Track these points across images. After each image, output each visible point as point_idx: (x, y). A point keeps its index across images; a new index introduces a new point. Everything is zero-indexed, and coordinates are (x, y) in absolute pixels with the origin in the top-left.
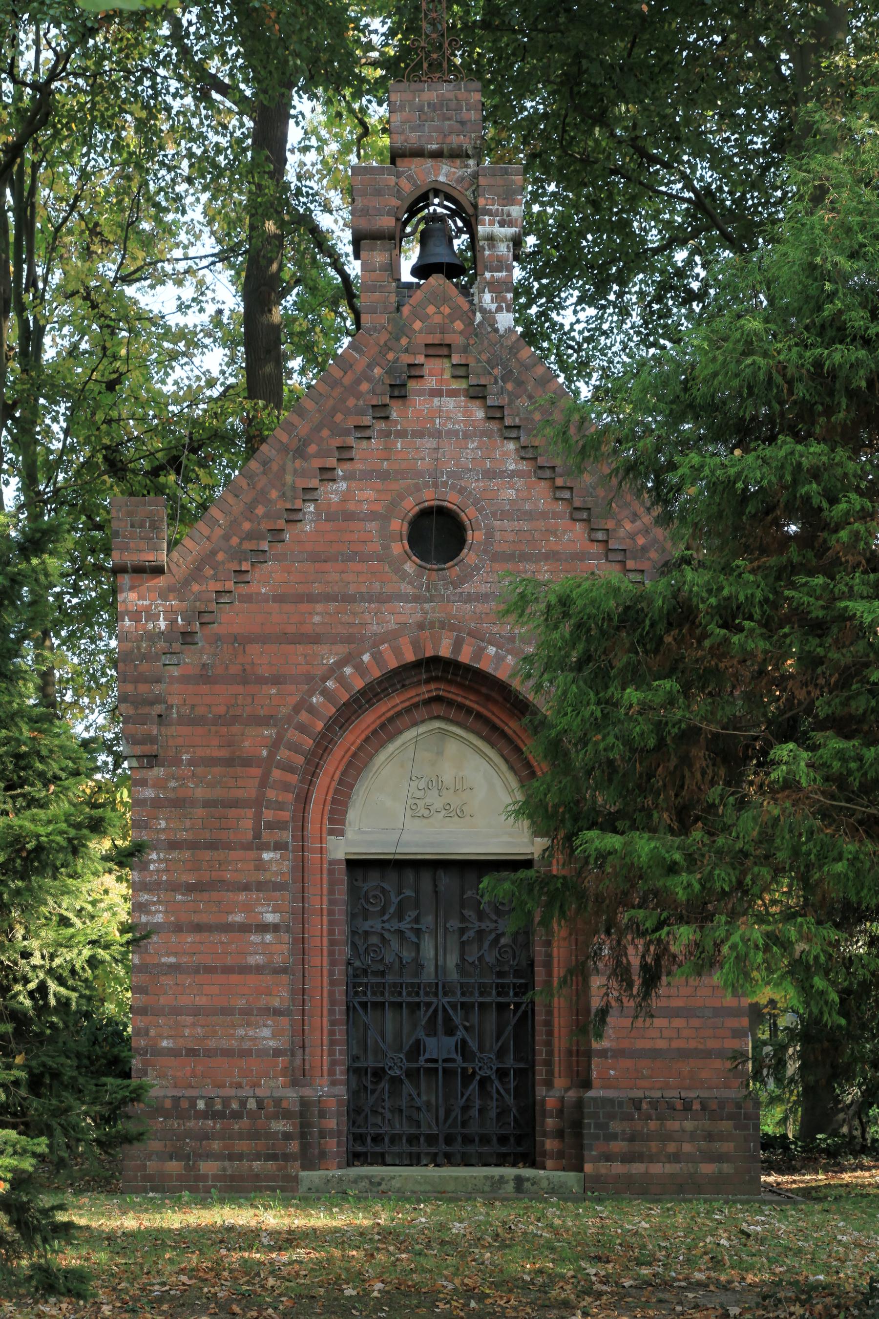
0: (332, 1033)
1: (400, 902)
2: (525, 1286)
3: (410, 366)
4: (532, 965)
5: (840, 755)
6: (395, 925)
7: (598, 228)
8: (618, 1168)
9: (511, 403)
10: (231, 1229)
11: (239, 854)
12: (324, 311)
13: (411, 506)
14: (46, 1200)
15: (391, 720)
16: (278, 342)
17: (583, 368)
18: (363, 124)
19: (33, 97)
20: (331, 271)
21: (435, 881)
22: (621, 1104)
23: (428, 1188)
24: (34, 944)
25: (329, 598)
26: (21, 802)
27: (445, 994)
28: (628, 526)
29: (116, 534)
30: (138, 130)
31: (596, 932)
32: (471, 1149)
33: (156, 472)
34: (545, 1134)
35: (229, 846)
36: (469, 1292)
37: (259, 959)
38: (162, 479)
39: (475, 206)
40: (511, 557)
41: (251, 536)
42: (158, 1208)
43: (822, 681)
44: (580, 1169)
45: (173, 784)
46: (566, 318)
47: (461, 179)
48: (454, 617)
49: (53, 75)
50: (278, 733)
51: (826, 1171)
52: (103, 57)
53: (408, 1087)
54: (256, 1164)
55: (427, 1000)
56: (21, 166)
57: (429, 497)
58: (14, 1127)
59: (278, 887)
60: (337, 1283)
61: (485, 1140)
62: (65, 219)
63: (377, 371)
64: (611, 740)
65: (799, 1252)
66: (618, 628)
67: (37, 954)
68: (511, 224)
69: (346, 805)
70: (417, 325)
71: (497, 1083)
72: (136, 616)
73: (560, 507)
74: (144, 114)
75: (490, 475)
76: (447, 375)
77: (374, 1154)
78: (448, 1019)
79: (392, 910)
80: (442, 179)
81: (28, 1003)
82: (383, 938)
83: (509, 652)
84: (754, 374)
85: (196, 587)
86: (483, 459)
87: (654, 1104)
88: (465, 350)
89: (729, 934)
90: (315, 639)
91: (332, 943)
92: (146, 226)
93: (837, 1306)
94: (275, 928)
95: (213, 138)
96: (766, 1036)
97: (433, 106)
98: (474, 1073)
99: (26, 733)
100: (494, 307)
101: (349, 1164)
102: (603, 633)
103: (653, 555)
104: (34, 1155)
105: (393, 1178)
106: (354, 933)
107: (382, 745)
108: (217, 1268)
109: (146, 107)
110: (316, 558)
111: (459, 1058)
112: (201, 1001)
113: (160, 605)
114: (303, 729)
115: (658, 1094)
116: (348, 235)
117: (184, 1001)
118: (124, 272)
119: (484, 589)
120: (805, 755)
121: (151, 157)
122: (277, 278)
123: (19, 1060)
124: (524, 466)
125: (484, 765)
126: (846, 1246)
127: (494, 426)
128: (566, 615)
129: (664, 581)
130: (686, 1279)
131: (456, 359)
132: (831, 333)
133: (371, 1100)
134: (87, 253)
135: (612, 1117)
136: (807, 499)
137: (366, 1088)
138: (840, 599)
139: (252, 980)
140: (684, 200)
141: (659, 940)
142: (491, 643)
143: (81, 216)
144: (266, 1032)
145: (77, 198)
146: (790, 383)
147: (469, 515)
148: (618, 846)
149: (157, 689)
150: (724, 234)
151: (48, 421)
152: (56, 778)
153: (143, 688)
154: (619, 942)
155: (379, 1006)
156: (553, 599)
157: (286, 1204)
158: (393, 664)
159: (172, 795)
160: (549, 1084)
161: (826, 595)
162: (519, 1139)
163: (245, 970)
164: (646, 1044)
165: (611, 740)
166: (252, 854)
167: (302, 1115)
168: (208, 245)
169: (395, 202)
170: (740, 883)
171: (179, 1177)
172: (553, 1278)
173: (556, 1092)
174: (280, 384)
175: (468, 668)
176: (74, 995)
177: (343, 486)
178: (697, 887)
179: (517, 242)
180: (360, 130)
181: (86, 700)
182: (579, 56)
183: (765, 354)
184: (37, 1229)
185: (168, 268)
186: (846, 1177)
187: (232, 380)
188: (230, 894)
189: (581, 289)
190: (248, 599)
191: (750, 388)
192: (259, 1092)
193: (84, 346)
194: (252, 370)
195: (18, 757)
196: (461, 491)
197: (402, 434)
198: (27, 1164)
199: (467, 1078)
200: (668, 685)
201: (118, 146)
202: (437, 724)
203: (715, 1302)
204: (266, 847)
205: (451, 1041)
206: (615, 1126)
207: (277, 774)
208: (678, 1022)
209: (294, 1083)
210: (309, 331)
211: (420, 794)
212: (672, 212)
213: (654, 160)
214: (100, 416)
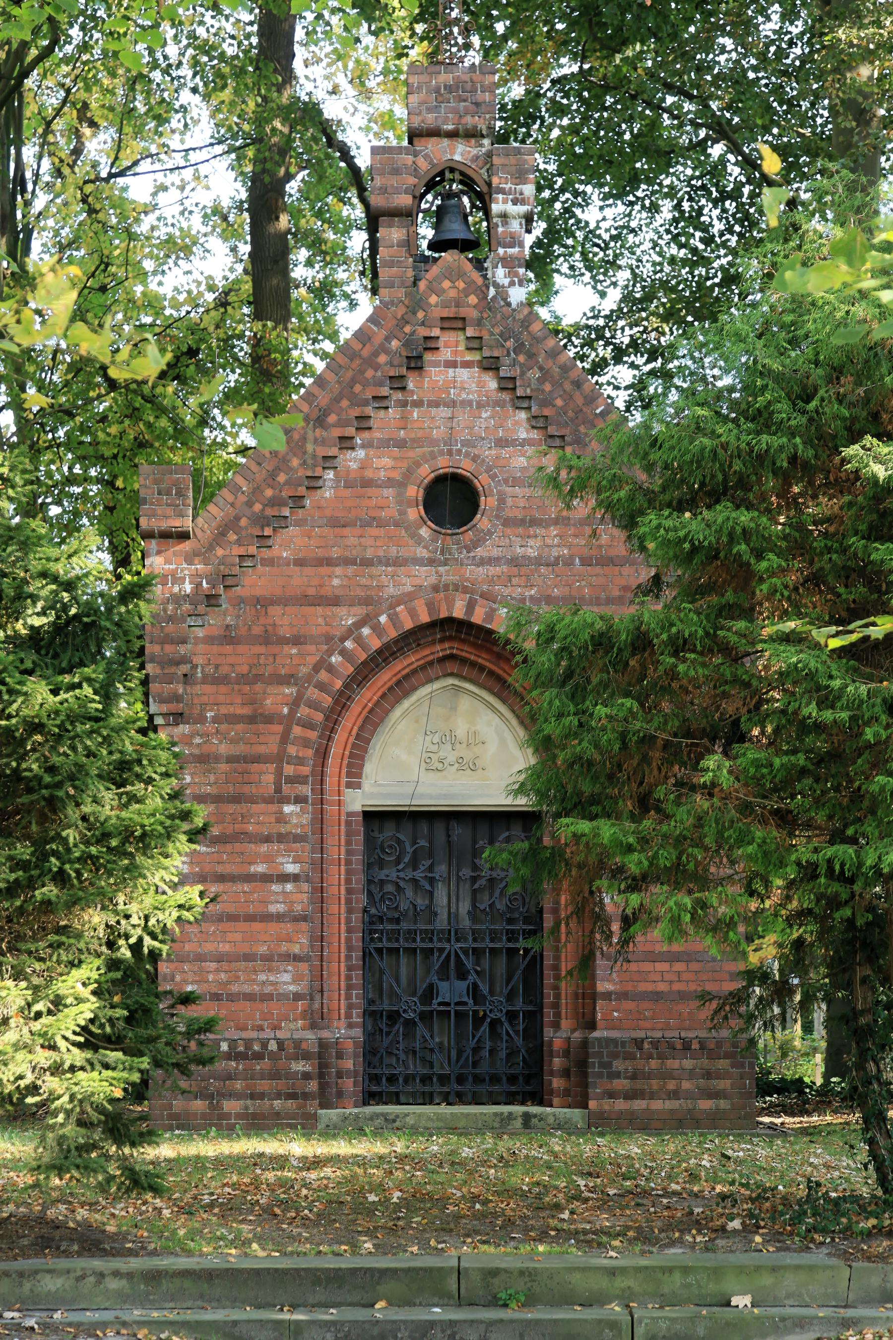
0: (349, 978)
1: (415, 852)
2: (524, 1195)
4: (541, 912)
6: (409, 874)
8: (621, 1105)
9: (523, 374)
10: (262, 1155)
11: (262, 807)
13: (426, 473)
15: (406, 677)
21: (448, 830)
22: (623, 1044)
23: (441, 1124)
24: (133, 908)
25: (349, 562)
27: (458, 940)
32: (482, 1088)
34: (552, 1073)
35: (252, 800)
36: (475, 1198)
37: (280, 908)
39: (489, 184)
40: (522, 522)
44: (586, 1106)
45: (198, 740)
46: (590, 215)
47: (476, 158)
48: (467, 580)
50: (298, 691)
53: (421, 1030)
54: (277, 1103)
55: (439, 945)
57: (443, 464)
59: (297, 838)
61: (495, 1079)
63: (395, 344)
64: (585, 744)
68: (523, 202)
69: (362, 758)
70: (433, 299)
71: (506, 1025)
75: (501, 443)
76: (461, 347)
78: (459, 963)
79: (406, 860)
80: (457, 157)
82: (399, 889)
85: (220, 552)
86: (496, 428)
87: (655, 1044)
88: (479, 323)
90: (335, 601)
91: (349, 891)
94: (295, 878)
97: (449, 88)
98: (485, 1015)
100: (506, 282)
101: (365, 1103)
105: (407, 1115)
106: (370, 882)
110: (336, 523)
111: (471, 1002)
112: (225, 948)
113: (186, 570)
114: (322, 687)
115: (659, 1034)
117: (209, 948)
119: (496, 552)
120: (727, 764)
124: (535, 435)
125: (496, 720)
127: (506, 396)
130: (664, 1189)
131: (470, 332)
135: (615, 1056)
137: (381, 1030)
139: (273, 928)
144: (287, 977)
147: (482, 481)
149: (182, 649)
153: (169, 648)
157: (308, 1136)
158: (409, 625)
159: (196, 752)
160: (556, 1025)
162: (528, 1080)
163: (267, 918)
166: (274, 808)
167: (320, 1055)
169: (412, 180)
171: (204, 1116)
173: (563, 1033)
175: (480, 628)
177: (361, 453)
188: (253, 846)
192: (280, 1035)
196: (475, 458)
197: (418, 404)
199: (478, 1021)
202: (451, 681)
204: (286, 800)
205: (462, 986)
206: (619, 1065)
207: (297, 731)
209: (313, 1026)
211: (434, 748)
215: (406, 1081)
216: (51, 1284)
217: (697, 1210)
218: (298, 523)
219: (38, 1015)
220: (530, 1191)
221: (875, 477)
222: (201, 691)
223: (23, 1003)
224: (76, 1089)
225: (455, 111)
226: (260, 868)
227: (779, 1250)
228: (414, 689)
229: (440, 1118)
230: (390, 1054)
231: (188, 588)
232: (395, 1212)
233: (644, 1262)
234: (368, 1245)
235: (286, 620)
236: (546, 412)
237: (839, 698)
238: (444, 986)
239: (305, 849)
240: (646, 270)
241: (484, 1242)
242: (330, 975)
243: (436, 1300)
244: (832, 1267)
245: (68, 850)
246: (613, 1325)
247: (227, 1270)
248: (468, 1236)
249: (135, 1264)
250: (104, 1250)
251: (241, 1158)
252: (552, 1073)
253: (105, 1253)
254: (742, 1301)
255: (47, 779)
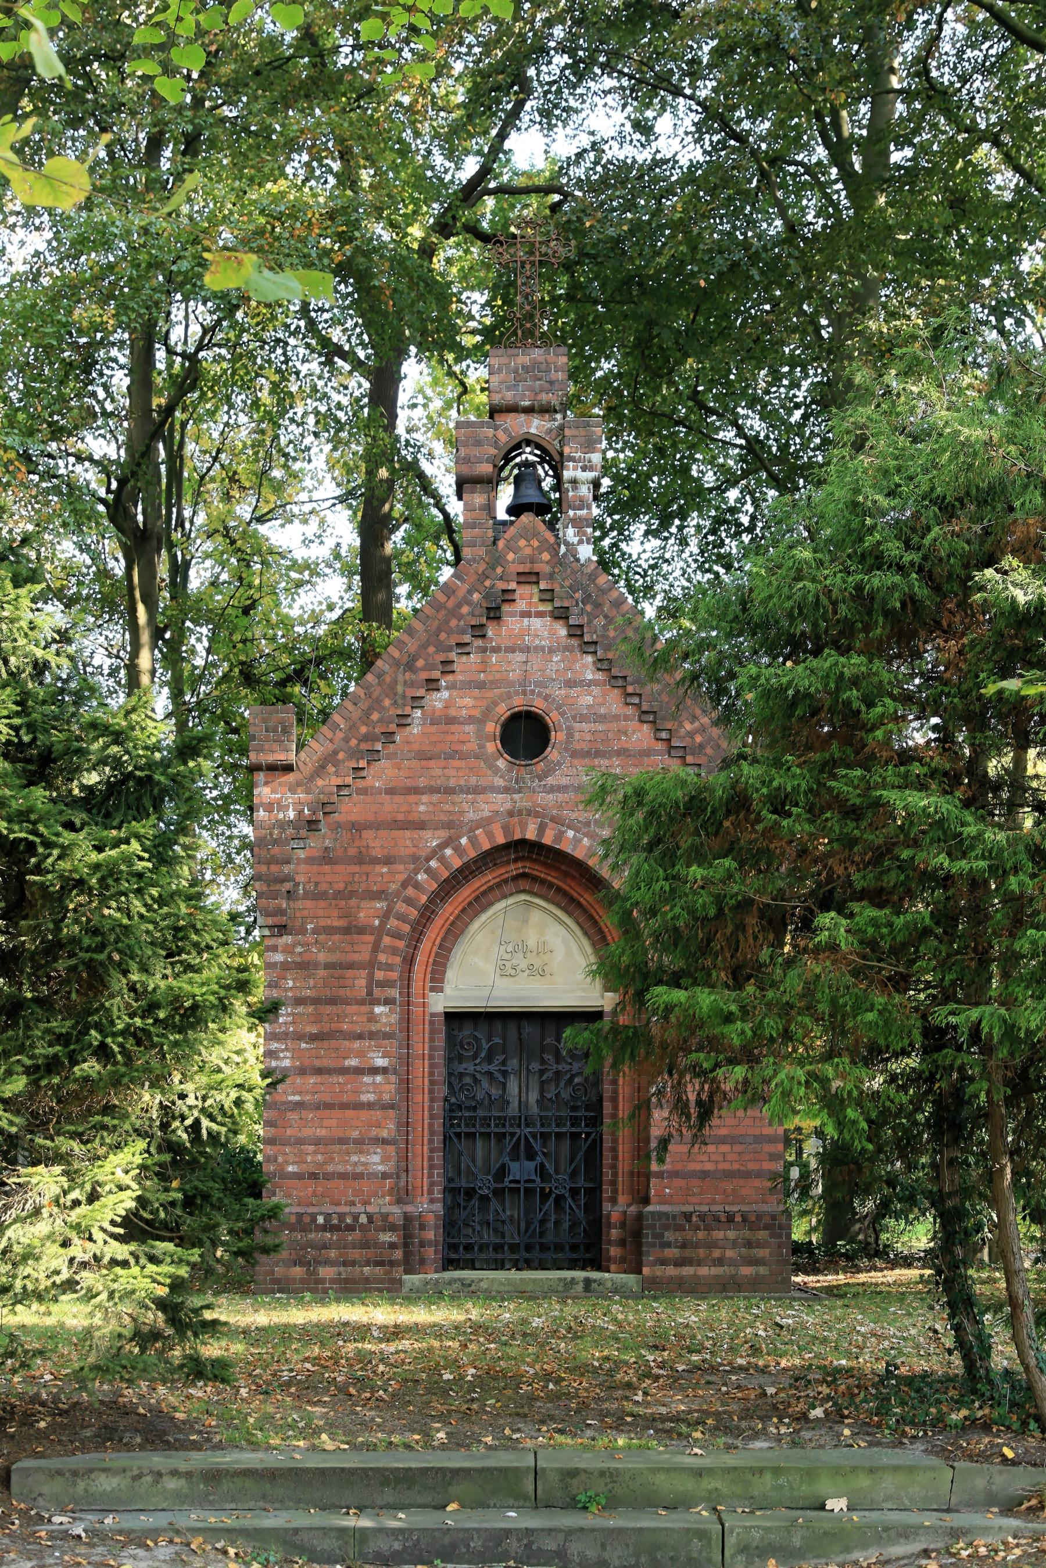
0: (431, 1159)
2: (595, 1371)
3: (504, 591)
4: (600, 1100)
5: (874, 922)
6: (485, 1068)
7: (661, 471)
8: (671, 1271)
9: (590, 622)
10: (346, 1324)
11: (355, 1008)
12: (428, 544)
13: (503, 711)
14: (196, 1301)
15: (484, 893)
16: (390, 572)
17: (648, 591)
18: (462, 384)
19: (183, 365)
20: (435, 511)
22: (674, 1217)
24: (189, 1087)
25: (433, 790)
26: (178, 968)
27: (527, 1125)
28: (688, 727)
29: (253, 738)
30: (272, 392)
31: (660, 1073)
33: (282, 683)
34: (609, 1243)
35: (346, 1002)
36: (548, 1377)
37: (371, 1097)
38: (289, 689)
39: (561, 454)
40: (588, 754)
41: (367, 738)
42: (285, 1306)
43: (857, 859)
44: (639, 1272)
45: (299, 949)
46: (632, 548)
47: (549, 431)
49: (200, 347)
51: (845, 1272)
52: (243, 330)
53: (494, 1204)
54: (366, 1269)
56: (172, 425)
57: (518, 703)
58: (171, 1240)
59: (387, 1036)
60: (436, 1370)
61: (559, 1247)
62: (209, 469)
63: (476, 596)
64: (677, 910)
65: (824, 1341)
66: (684, 815)
67: (192, 1096)
68: (591, 469)
69: (445, 966)
70: (511, 556)
72: (269, 808)
73: (630, 711)
74: (276, 378)
75: (570, 684)
76: (535, 599)
77: (466, 1261)
78: (529, 1146)
80: (533, 431)
81: (185, 1136)
82: (476, 1081)
83: (585, 835)
84: (804, 597)
85: (320, 782)
86: (566, 670)
87: (702, 1217)
88: (551, 577)
89: (776, 1073)
90: (421, 826)
91: (432, 1083)
92: (277, 473)
93: (858, 1387)
94: (384, 1071)
95: (336, 397)
96: (792, 1159)
97: (526, 369)
99: (184, 910)
100: (576, 540)
101: (445, 1269)
102: (671, 819)
103: (709, 751)
104: (188, 1263)
106: (450, 1075)
107: (476, 915)
108: (335, 1359)
109: (279, 371)
110: (423, 756)
112: (321, 1132)
113: (290, 798)
114: (409, 901)
115: (705, 1208)
116: (451, 479)
117: (307, 1132)
118: (258, 514)
119: (564, 781)
120: (844, 922)
121: (282, 414)
122: (388, 516)
123: (175, 1184)
124: (600, 676)
125: (562, 931)
126: (864, 1336)
127: (575, 642)
128: (640, 804)
129: (724, 774)
130: (730, 1364)
131: (543, 585)
132: (870, 561)
133: (464, 1214)
134: (227, 497)
135: (667, 1228)
136: (848, 703)
138: (875, 788)
139: (364, 1115)
140: (736, 446)
141: (713, 1080)
142: (569, 827)
143: (222, 466)
144: (376, 1158)
145: (219, 451)
146: (834, 604)
147: (553, 718)
148: (683, 999)
149: (286, 869)
150: (770, 474)
151: (193, 641)
152: (209, 947)
153: (274, 868)
154: (679, 1083)
155: (471, 1136)
156: (629, 790)
157: (392, 1301)
158: (486, 846)
159: (298, 959)
160: (614, 1200)
161: (862, 785)
163: (359, 1106)
164: (698, 1167)
165: (677, 910)
166: (365, 1008)
167: (405, 1227)
168: (330, 490)
169: (493, 451)
170: (786, 1030)
171: (302, 1281)
172: (618, 1364)
173: (620, 1207)
174: (390, 608)
175: (550, 849)
176: (224, 1129)
177: (445, 694)
178: (749, 1033)
179: (596, 484)
180: (460, 389)
181: (222, 878)
182: (650, 324)
183: (814, 580)
184: (189, 1326)
185: (296, 509)
186: (862, 1277)
187: (349, 605)
189: (648, 524)
190: (364, 791)
191: (800, 608)
192: (370, 1209)
193: (224, 577)
194: (366, 595)
195: (177, 929)
196: (546, 698)
197: (496, 650)
198: (183, 1272)
199: (545, 1196)
200: (728, 863)
201: (256, 404)
203: (754, 1383)
204: (378, 1002)
205: (531, 1165)
206: (670, 1236)
207: (387, 940)
208: (724, 1148)
209: (399, 1201)
210: (415, 561)
211: (508, 956)
212: (726, 457)
213: (712, 411)
214: (237, 637)
215: (481, 1249)
216: (106, 1484)
217: (771, 1391)
218: (389, 757)
219: (76, 1203)
220: (600, 1367)
221: (1014, 600)
222: (303, 906)
223: (58, 1191)
224: (116, 1286)
225: (531, 389)
226: (353, 1062)
227: (871, 1444)
228: (491, 904)
229: (509, 1282)
230: (467, 1225)
231: (291, 814)
232: (469, 1392)
233: (730, 1460)
234: (441, 1435)
235: (378, 843)
236: (610, 656)
237: (972, 847)
238: (514, 1166)
239: (392, 1046)
240: (678, 592)
241: (561, 1432)
242: (414, 1156)
243: (511, 1502)
244: (933, 1469)
245: (112, 1023)
246: (702, 1534)
247: (291, 1469)
248: (543, 1422)
249: (197, 1460)
250: (168, 1442)
251: (329, 1325)
252: (609, 1243)
253: (169, 1446)
254: (837, 1504)
255: (86, 941)
